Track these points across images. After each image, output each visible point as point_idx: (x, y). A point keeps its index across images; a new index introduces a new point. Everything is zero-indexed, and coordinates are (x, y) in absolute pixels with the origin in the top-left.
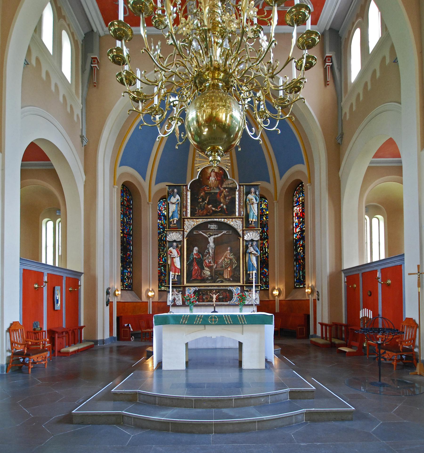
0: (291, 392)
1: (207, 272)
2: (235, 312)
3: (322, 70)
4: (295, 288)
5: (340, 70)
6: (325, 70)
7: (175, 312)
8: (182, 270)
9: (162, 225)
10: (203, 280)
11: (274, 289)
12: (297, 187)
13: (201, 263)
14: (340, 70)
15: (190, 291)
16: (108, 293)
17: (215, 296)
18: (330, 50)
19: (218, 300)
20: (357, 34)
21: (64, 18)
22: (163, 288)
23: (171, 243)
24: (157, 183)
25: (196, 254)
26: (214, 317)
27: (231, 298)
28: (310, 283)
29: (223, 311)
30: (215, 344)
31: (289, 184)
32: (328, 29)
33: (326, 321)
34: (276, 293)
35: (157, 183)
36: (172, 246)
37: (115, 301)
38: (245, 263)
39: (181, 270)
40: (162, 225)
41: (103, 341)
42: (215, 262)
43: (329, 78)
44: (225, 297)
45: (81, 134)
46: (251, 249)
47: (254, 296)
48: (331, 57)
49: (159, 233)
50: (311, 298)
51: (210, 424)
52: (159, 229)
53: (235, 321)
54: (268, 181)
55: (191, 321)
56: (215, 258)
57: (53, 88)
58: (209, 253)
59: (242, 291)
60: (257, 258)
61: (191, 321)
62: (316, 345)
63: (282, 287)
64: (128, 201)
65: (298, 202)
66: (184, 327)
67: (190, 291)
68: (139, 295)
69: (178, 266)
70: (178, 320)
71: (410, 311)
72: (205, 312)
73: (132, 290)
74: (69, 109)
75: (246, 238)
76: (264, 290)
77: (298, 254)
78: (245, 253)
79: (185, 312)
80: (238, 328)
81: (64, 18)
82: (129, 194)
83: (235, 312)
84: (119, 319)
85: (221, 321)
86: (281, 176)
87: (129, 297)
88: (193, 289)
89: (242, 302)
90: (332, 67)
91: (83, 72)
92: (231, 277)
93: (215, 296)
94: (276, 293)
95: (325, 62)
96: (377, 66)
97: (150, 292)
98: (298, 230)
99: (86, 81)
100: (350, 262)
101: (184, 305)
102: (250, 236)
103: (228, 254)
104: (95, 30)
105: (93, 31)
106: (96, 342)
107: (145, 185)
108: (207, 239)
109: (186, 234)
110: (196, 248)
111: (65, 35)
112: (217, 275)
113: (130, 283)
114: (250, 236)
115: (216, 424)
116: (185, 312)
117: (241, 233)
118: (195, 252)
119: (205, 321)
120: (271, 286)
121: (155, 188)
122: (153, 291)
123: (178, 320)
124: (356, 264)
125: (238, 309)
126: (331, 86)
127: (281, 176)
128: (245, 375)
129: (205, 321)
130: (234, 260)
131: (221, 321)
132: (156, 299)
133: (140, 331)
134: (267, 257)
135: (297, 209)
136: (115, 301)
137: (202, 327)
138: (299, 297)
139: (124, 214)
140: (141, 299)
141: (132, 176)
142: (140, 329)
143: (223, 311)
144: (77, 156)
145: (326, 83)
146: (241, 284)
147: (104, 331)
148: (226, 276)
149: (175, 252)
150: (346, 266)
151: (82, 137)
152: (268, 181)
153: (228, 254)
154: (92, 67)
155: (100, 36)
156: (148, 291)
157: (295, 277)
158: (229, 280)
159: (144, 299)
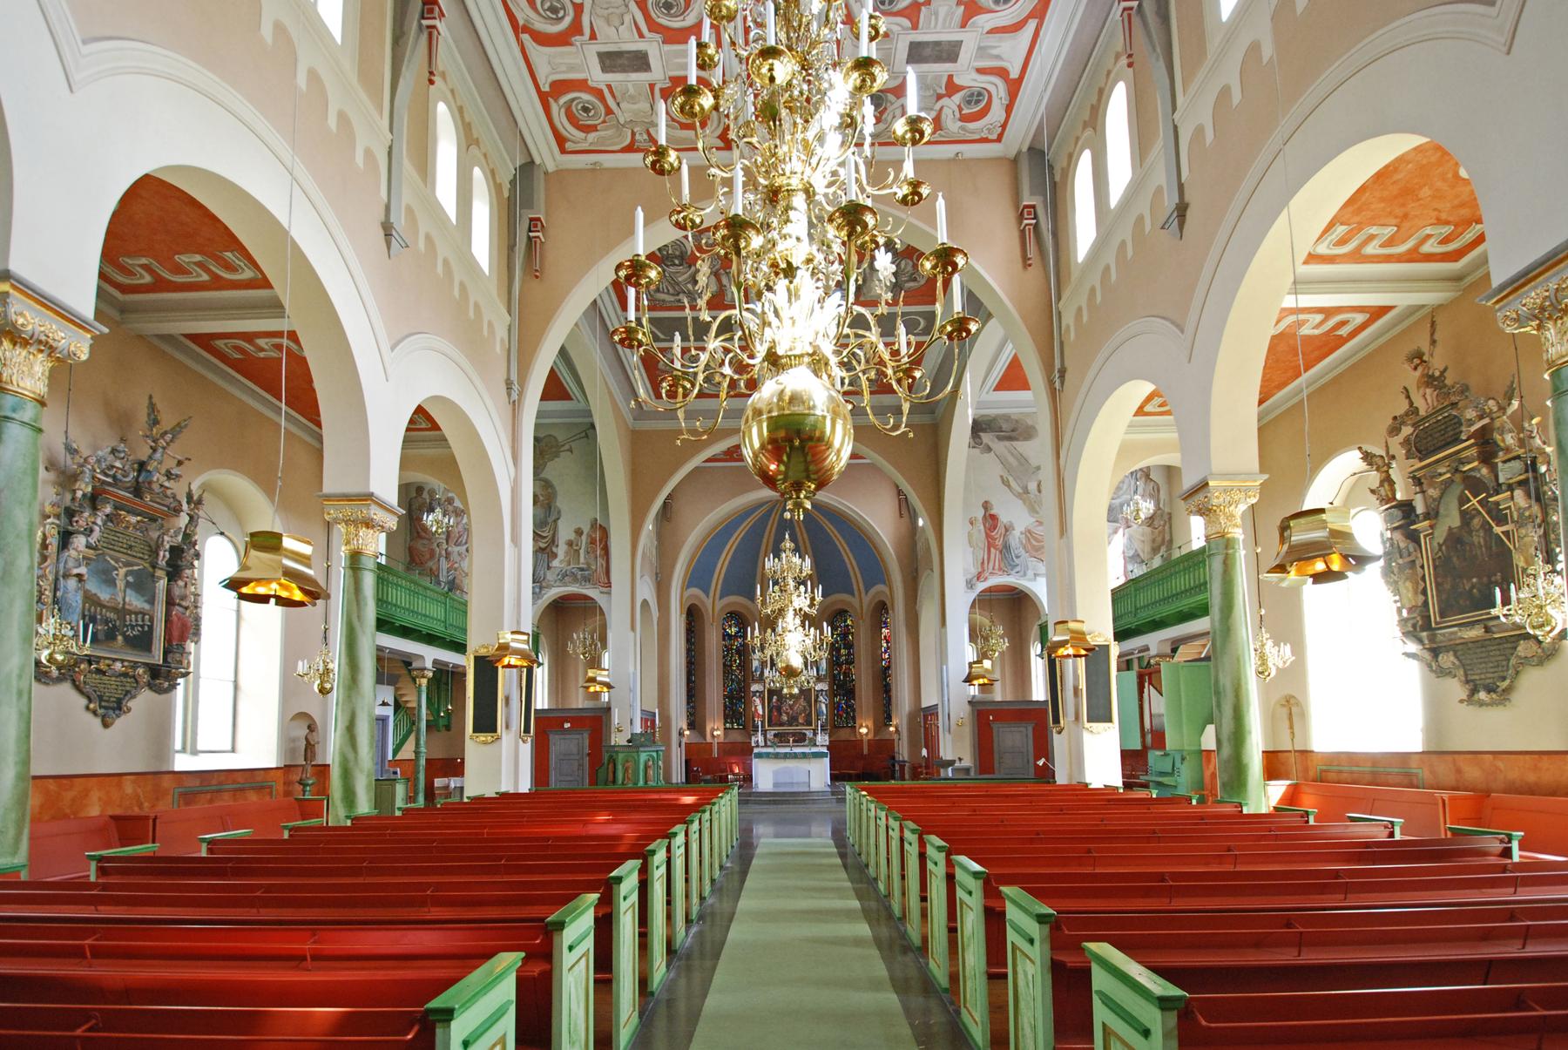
1: (785, 718)
2: (806, 750)
3: (1016, 234)
6: (1022, 232)
10: (782, 724)
13: (779, 709)
15: (770, 735)
20: (1085, 161)
21: (477, 142)
28: (894, 722)
32: (1025, 149)
34: (864, 730)
43: (1032, 251)
44: (800, 739)
45: (383, 218)
47: (823, 739)
48: (1033, 207)
50: (895, 737)
53: (804, 756)
55: (777, 756)
57: (267, 31)
63: (870, 724)
68: (703, 735)
70: (768, 755)
72: (787, 750)
74: (456, 293)
79: (770, 750)
81: (477, 142)
82: (693, 615)
83: (806, 750)
85: (795, 756)
87: (696, 739)
90: (1036, 226)
95: (1021, 217)
96: (1125, 233)
97: (716, 730)
101: (766, 746)
102: (819, 687)
104: (538, 161)
105: (533, 162)
107: (709, 602)
111: (477, 172)
112: (793, 720)
113: (695, 723)
116: (770, 750)
121: (719, 604)
123: (768, 755)
126: (1035, 271)
129: (785, 756)
136: (684, 740)
141: (697, 597)
145: (901, 515)
149: (758, 701)
150: (924, 705)
154: (529, 238)
155: (546, 173)
156: (713, 730)
159: (709, 739)
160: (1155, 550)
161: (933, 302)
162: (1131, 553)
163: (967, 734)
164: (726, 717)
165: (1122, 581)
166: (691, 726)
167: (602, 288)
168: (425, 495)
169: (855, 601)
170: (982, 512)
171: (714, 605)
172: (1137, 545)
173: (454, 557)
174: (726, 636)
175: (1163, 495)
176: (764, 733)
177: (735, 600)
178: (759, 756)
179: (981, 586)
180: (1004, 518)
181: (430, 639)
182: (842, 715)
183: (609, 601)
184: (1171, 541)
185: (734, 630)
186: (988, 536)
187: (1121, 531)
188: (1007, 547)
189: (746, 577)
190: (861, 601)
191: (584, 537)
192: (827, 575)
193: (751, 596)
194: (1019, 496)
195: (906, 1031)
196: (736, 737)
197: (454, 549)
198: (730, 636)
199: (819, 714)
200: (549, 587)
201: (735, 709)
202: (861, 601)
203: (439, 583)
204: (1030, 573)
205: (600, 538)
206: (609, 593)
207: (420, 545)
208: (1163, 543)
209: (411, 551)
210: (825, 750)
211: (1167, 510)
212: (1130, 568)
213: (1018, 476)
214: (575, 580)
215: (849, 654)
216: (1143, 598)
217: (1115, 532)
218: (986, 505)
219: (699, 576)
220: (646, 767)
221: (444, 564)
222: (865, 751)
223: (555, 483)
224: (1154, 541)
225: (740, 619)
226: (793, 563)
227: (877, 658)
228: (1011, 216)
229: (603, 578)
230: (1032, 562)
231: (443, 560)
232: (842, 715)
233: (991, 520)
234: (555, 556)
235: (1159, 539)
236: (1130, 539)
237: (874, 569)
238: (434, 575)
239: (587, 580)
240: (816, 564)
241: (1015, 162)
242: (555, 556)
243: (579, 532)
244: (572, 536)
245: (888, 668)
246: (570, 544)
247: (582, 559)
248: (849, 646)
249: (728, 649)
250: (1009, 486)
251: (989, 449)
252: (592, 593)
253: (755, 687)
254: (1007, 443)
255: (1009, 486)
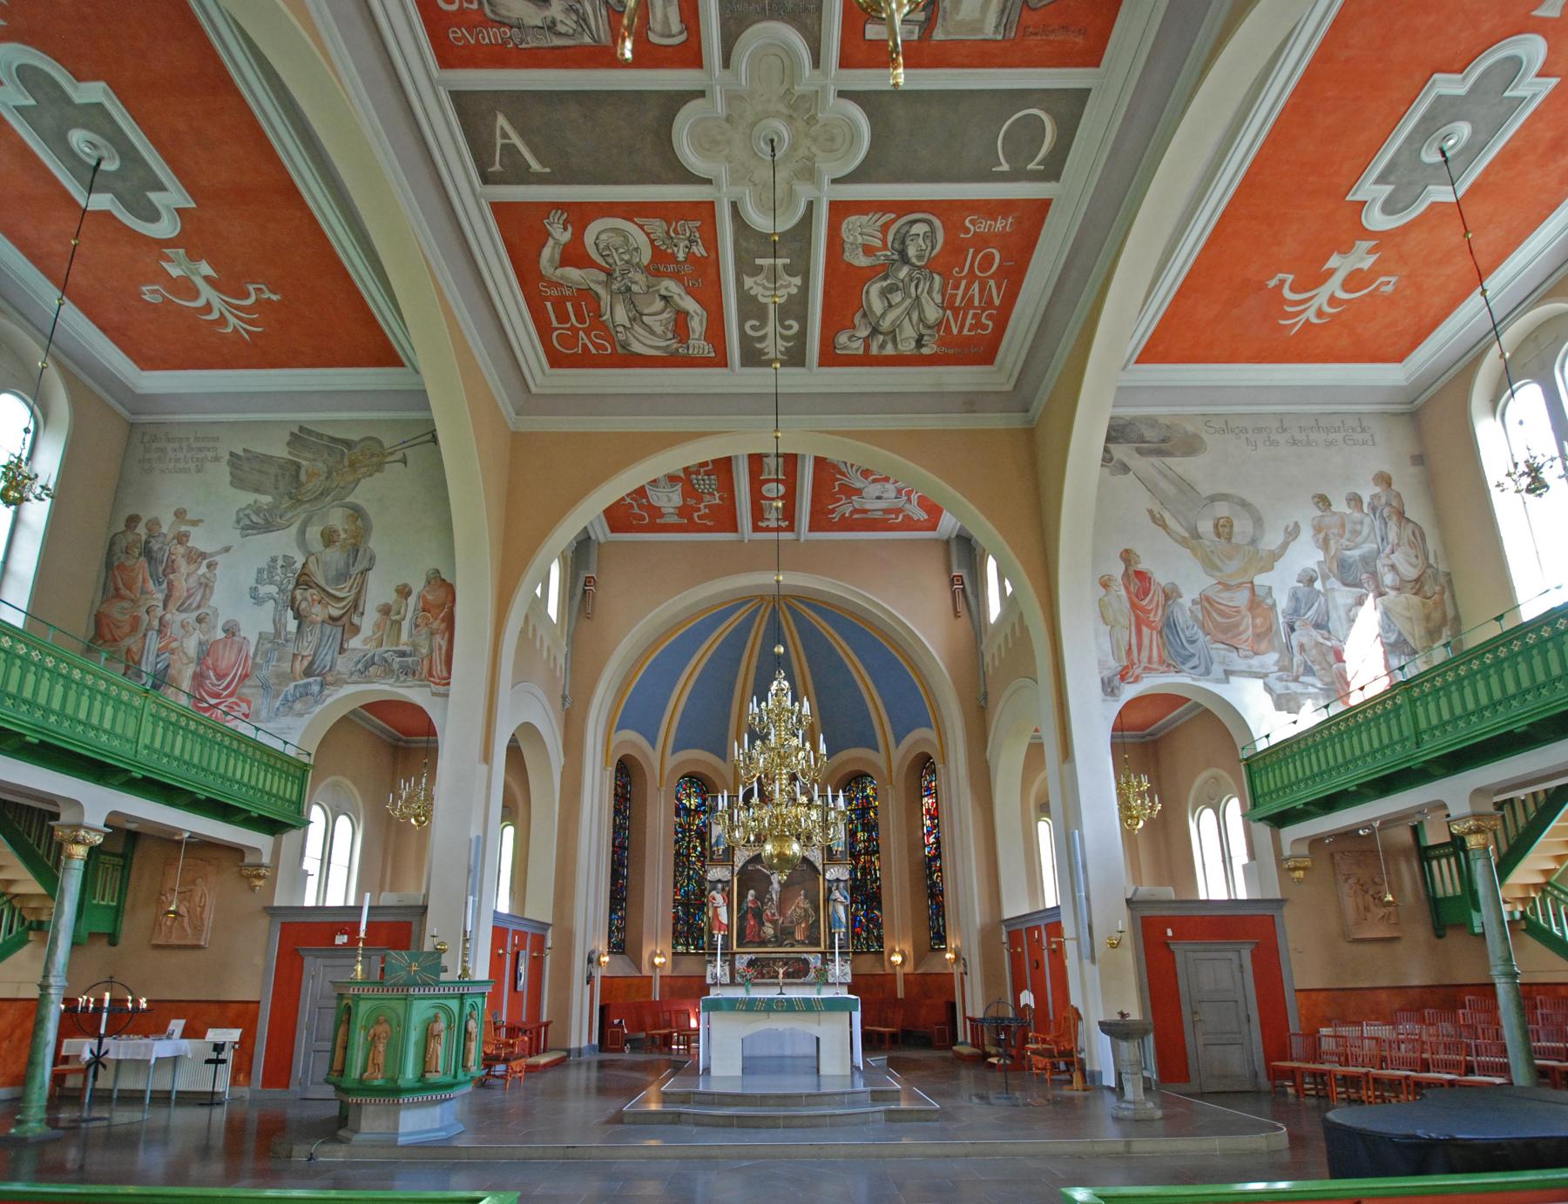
0: (873, 1092)
1: (769, 930)
3: (949, 595)
4: (933, 949)
5: (977, 597)
6: (953, 593)
7: (714, 993)
8: (729, 927)
9: (681, 825)
11: (893, 951)
12: (924, 765)
13: (758, 914)
14: (977, 597)
15: (741, 962)
16: (590, 961)
17: (781, 971)
18: (959, 567)
19: (787, 975)
22: (680, 949)
23: (714, 883)
24: (674, 752)
25: (753, 902)
26: (781, 1000)
27: (806, 974)
28: (953, 942)
29: (794, 993)
30: (780, 1035)
31: (907, 763)
33: (979, 1014)
34: (897, 959)
35: (674, 752)
36: (714, 889)
37: (598, 974)
38: (827, 916)
39: (729, 927)
40: (681, 825)
41: (579, 1051)
42: (781, 913)
43: (961, 607)
44: (798, 971)
46: (836, 894)
47: (840, 970)
49: (677, 842)
50: (957, 970)
51: (778, 1117)
52: (676, 833)
53: (808, 1006)
54: (876, 749)
55: (750, 1006)
56: (781, 908)
58: (771, 899)
59: (825, 961)
60: (846, 908)
61: (750, 1006)
62: (961, 1058)
63: (908, 948)
64: (624, 786)
65: (928, 789)
66: (743, 1015)
67: (741, 962)
69: (725, 921)
70: (732, 1005)
71: (1075, 999)
72: (771, 993)
73: (623, 953)
75: (828, 876)
76: (876, 953)
77: (934, 884)
78: (827, 900)
79: (739, 993)
80: (813, 1016)
82: (627, 773)
84: (602, 1009)
85: (790, 1006)
86: (898, 743)
87: (621, 968)
88: (746, 958)
89: (823, 980)
90: (963, 590)
91: (572, 598)
92: (808, 937)
93: (781, 971)
94: (897, 959)
95: (952, 584)
97: (658, 956)
98: (932, 840)
99: (575, 609)
100: (1015, 907)
101: (733, 983)
102: (833, 873)
103: (801, 902)
106: (569, 1051)
107: (655, 757)
108: (768, 878)
109: (736, 869)
110: (752, 892)
114: (833, 873)
115: (785, 1117)
116: (739, 993)
117: (820, 868)
118: (750, 897)
119: (769, 1007)
120: (887, 945)
121: (672, 761)
122: (662, 954)
123: (732, 1005)
124: (1025, 909)
125: (815, 990)
126: (964, 619)
127: (898, 743)
128: (823, 1081)
129: (769, 1007)
130: (811, 911)
131: (790, 1006)
132: (668, 972)
133: (643, 1035)
134: (879, 888)
135: (928, 802)
136: (598, 974)
137: (764, 1015)
138: (938, 969)
139: (617, 812)
140: (640, 970)
141: (634, 745)
142: (643, 1030)
143: (794, 993)
144: (554, 722)
145: (956, 614)
146: (822, 949)
147: (581, 1033)
148: (798, 936)
151: (564, 697)
152: (876, 749)
153: (801, 902)
154: (585, 591)
156: (654, 954)
157: (931, 928)
158: (802, 943)
159: (646, 971)
160: (1433, 634)
161: (1091, 56)
162: (1393, 638)
163: (1128, 959)
164: (676, 935)
165: (1382, 685)
166: (617, 948)
167: (592, 517)
168: (141, 530)
169: (879, 759)
170: (1121, 567)
171: (663, 762)
172: (1401, 625)
173: (175, 630)
174: (680, 810)
175: (1431, 544)
176: (730, 958)
177: (698, 757)
178: (716, 1006)
179: (1130, 692)
180: (1161, 578)
181: (97, 770)
182: (866, 934)
183: (445, 708)
184: (1457, 619)
185: (694, 801)
186: (1134, 606)
187: (1370, 601)
188: (1170, 624)
189: (712, 723)
190: (889, 758)
191: (412, 600)
192: (839, 722)
193: (722, 752)
194: (1183, 542)
195: (788, 1052)
196: (689, 967)
197: (175, 618)
198: (688, 811)
199: (831, 923)
200: (339, 682)
201: (689, 926)
202: (889, 758)
203: (139, 675)
204: (1217, 669)
205: (441, 602)
206: (446, 695)
207: (116, 611)
208: (1444, 622)
209: (99, 620)
210: (843, 993)
211: (1442, 568)
212: (1395, 663)
213: (1179, 509)
214: (388, 672)
215: (870, 839)
216: (1429, 714)
217: (1360, 602)
218: (1127, 556)
219: (638, 710)
220: (429, 1035)
221: (153, 642)
222: (900, 994)
223: (371, 510)
224: (1428, 618)
225: (701, 783)
226: (783, 706)
227: (916, 844)
228: (945, 581)
229: (439, 668)
230: (1218, 651)
231: (152, 635)
232: (866, 934)
233: (1139, 581)
234: (356, 630)
235: (1437, 615)
236: (1386, 614)
237: (911, 707)
238: (132, 668)
239: (409, 671)
240: (821, 707)
241: (947, 542)
242: (356, 630)
243: (404, 592)
244: (391, 597)
245: (938, 856)
246: (386, 610)
247: (404, 637)
248: (870, 827)
249: (684, 829)
250: (1164, 526)
251: (1125, 469)
252: (415, 694)
253: (716, 873)
254: (1154, 460)
255: (1164, 526)
